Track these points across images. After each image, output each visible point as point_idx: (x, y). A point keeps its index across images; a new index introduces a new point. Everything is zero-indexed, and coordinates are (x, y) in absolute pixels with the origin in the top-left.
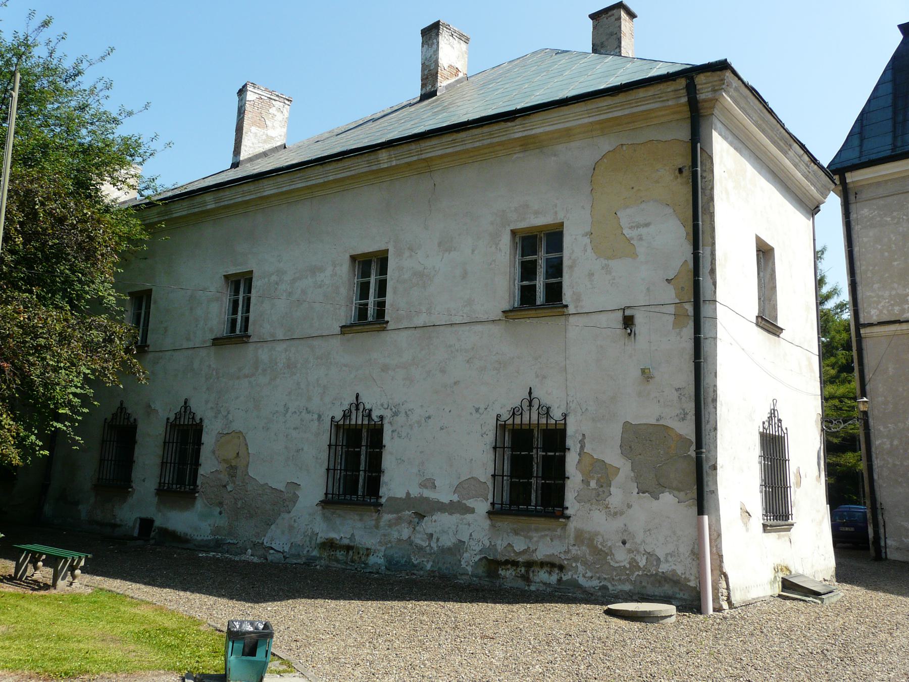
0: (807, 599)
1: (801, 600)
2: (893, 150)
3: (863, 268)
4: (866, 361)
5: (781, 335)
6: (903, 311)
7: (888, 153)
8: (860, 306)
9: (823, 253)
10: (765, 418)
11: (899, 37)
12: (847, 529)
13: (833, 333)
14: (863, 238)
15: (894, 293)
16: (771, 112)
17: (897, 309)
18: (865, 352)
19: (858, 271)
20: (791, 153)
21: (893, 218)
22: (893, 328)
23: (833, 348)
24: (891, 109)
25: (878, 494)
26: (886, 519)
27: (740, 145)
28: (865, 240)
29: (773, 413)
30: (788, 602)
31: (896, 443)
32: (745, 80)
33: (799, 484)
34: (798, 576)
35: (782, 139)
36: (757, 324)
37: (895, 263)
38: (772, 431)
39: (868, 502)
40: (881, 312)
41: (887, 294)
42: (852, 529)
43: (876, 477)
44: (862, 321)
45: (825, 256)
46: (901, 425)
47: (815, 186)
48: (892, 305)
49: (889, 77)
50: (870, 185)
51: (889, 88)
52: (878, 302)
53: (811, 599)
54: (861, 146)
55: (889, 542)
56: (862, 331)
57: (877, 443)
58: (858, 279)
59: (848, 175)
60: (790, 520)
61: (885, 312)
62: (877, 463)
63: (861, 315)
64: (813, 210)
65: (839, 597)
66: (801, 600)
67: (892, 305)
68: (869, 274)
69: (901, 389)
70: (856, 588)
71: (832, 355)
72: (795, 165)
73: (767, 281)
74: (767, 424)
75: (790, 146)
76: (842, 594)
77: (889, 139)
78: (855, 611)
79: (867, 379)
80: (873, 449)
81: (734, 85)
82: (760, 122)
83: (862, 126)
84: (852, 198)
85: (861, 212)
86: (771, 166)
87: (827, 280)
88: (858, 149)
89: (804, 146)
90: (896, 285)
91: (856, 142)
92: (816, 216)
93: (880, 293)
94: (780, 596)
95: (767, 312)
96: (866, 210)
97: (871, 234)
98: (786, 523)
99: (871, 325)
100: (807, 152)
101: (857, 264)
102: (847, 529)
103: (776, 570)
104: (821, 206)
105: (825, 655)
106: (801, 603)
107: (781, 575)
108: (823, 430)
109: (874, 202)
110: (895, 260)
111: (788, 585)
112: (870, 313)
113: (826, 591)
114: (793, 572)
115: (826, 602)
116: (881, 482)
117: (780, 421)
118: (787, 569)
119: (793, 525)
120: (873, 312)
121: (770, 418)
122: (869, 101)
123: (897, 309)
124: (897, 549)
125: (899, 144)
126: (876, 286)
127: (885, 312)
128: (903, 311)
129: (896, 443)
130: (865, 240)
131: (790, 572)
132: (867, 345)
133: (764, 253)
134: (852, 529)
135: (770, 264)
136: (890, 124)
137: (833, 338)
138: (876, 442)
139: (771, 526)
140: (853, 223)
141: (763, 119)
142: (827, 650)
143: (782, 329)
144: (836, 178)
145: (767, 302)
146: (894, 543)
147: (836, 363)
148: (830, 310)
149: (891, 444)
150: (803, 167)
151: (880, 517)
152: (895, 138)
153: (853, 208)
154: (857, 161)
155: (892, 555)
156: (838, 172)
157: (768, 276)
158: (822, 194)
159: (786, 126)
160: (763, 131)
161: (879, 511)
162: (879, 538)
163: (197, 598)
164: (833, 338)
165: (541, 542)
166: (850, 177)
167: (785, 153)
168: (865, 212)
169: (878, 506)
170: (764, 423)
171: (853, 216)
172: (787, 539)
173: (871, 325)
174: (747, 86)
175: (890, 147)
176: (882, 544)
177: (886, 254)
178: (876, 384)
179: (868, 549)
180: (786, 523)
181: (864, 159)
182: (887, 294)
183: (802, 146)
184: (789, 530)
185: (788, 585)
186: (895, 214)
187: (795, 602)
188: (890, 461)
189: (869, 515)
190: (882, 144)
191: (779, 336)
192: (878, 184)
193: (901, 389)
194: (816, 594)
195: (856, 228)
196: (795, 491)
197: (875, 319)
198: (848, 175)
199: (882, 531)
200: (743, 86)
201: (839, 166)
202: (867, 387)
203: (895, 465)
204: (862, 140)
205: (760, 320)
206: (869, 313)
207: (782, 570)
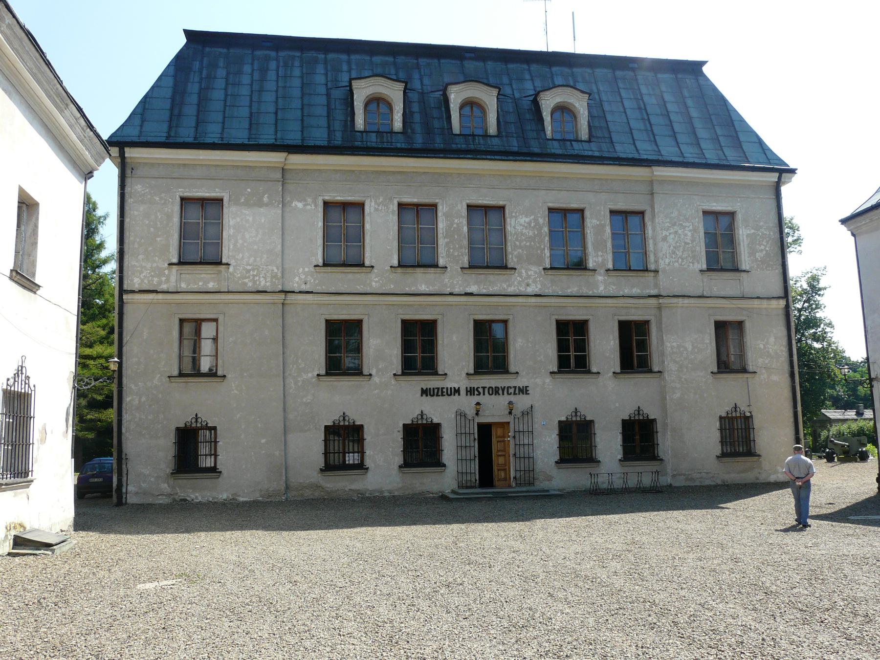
0: (37, 552)
1: (31, 554)
2: (195, 138)
3: (132, 238)
4: (125, 325)
5: (38, 292)
6: (160, 283)
7: (163, 140)
8: (125, 273)
9: (105, 219)
10: (11, 375)
11: (183, 41)
12: (96, 480)
13: (107, 296)
14: (134, 211)
15: (155, 265)
16: (48, 64)
17: (156, 279)
18: (125, 317)
19: (126, 241)
20: (67, 113)
21: (161, 199)
22: (151, 296)
23: (106, 310)
24: (169, 101)
25: (124, 446)
26: (129, 467)
27: (10, 88)
28: (136, 213)
29: (20, 370)
30: (17, 559)
31: (143, 399)
32: (21, 20)
33: (43, 440)
34: (33, 531)
35: (59, 95)
36: (11, 278)
37: (158, 239)
38: (18, 388)
39: (115, 454)
40: (142, 280)
41: (149, 265)
42: (101, 480)
43: (124, 430)
44: (125, 287)
45: (106, 222)
46: (149, 384)
47: (89, 152)
48: (152, 276)
49: (172, 71)
50: (146, 164)
51: (170, 82)
52: (141, 272)
53: (42, 551)
54: (141, 126)
55: (130, 488)
56: (125, 297)
57: (128, 399)
58: (126, 247)
59: (127, 150)
60: (30, 477)
61: (146, 281)
62: (126, 417)
63: (125, 282)
64: (87, 175)
65: (72, 545)
66: (31, 554)
67: (152, 276)
68: (136, 246)
69: (152, 352)
70: (91, 533)
71: (104, 317)
72: (71, 126)
73: (28, 234)
74: (12, 381)
75: (67, 105)
76: (75, 542)
77: (165, 127)
78: (83, 555)
79: (125, 341)
80: (124, 405)
81: (7, 22)
82: (34, 70)
83: (144, 109)
84: (128, 172)
85: (135, 187)
86: (45, 120)
87: (106, 245)
88: (138, 128)
89: (81, 110)
90: (157, 259)
91: (137, 121)
92: (89, 181)
93: (144, 264)
94: (9, 554)
95: (25, 267)
96: (139, 186)
97: (141, 209)
98: (25, 480)
99: (133, 292)
100: (84, 116)
101: (127, 234)
102: (96, 480)
103: (8, 529)
104: (95, 173)
105: (41, 604)
106: (31, 557)
107: (14, 532)
108: (74, 387)
109: (148, 180)
110: (159, 237)
111: (20, 542)
112: (134, 281)
113: (58, 541)
114: (28, 528)
115: (57, 552)
116: (127, 435)
117: (28, 378)
118: (21, 525)
119: (32, 481)
120: (136, 280)
121: (16, 375)
122: (153, 87)
123: (156, 279)
124: (137, 493)
125: (173, 134)
126: (141, 257)
127: (146, 281)
128: (160, 283)
129: (143, 399)
130: (136, 213)
131: (25, 528)
132: (127, 309)
133: (27, 207)
134: (101, 480)
135: (34, 219)
136: (168, 113)
137: (106, 301)
138: (127, 399)
139: (6, 484)
140: (127, 196)
141: (39, 69)
142: (44, 598)
143: (39, 286)
144: (115, 151)
145: (26, 257)
146: (133, 489)
147: (107, 324)
148: (106, 274)
149: (140, 401)
150: (78, 130)
151: (124, 466)
152: (170, 127)
153: (128, 181)
154: (136, 139)
155: (132, 499)
156: (119, 144)
157: (30, 230)
158: (96, 161)
159: (64, 84)
160: (39, 82)
161: (124, 462)
162: (122, 485)
163: (611, 516)
164: (106, 301)
165: (197, 490)
166: (130, 152)
167: (61, 111)
168: (139, 188)
169: (124, 456)
170: (8, 380)
171: (128, 189)
172: (25, 496)
173: (133, 292)
174: (22, 28)
175: (165, 135)
176: (124, 490)
177: (152, 229)
178: (132, 348)
179: (111, 496)
180: (25, 480)
181: (143, 139)
182: (149, 265)
183: (80, 110)
184: (28, 487)
185: (20, 542)
186: (163, 195)
187: (25, 558)
188: (137, 415)
189: (115, 466)
190: (158, 130)
191: (35, 293)
192: (152, 165)
193: (152, 352)
194: (48, 546)
195: (129, 201)
196: (39, 448)
197: (136, 287)
198: (127, 150)
199: (124, 479)
200: (18, 27)
201: (120, 139)
202: (124, 349)
203: (140, 419)
204: (143, 121)
205: (14, 274)
206: (132, 280)
207: (15, 528)
